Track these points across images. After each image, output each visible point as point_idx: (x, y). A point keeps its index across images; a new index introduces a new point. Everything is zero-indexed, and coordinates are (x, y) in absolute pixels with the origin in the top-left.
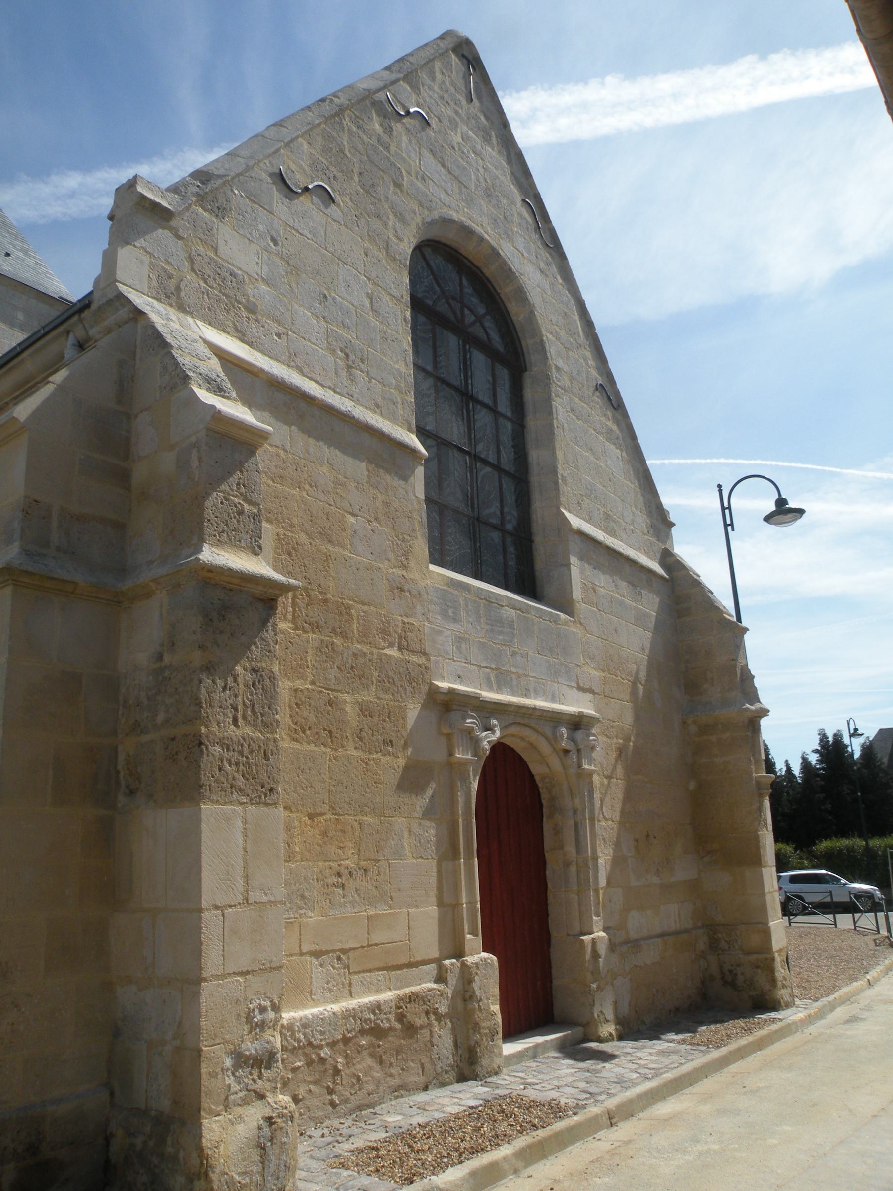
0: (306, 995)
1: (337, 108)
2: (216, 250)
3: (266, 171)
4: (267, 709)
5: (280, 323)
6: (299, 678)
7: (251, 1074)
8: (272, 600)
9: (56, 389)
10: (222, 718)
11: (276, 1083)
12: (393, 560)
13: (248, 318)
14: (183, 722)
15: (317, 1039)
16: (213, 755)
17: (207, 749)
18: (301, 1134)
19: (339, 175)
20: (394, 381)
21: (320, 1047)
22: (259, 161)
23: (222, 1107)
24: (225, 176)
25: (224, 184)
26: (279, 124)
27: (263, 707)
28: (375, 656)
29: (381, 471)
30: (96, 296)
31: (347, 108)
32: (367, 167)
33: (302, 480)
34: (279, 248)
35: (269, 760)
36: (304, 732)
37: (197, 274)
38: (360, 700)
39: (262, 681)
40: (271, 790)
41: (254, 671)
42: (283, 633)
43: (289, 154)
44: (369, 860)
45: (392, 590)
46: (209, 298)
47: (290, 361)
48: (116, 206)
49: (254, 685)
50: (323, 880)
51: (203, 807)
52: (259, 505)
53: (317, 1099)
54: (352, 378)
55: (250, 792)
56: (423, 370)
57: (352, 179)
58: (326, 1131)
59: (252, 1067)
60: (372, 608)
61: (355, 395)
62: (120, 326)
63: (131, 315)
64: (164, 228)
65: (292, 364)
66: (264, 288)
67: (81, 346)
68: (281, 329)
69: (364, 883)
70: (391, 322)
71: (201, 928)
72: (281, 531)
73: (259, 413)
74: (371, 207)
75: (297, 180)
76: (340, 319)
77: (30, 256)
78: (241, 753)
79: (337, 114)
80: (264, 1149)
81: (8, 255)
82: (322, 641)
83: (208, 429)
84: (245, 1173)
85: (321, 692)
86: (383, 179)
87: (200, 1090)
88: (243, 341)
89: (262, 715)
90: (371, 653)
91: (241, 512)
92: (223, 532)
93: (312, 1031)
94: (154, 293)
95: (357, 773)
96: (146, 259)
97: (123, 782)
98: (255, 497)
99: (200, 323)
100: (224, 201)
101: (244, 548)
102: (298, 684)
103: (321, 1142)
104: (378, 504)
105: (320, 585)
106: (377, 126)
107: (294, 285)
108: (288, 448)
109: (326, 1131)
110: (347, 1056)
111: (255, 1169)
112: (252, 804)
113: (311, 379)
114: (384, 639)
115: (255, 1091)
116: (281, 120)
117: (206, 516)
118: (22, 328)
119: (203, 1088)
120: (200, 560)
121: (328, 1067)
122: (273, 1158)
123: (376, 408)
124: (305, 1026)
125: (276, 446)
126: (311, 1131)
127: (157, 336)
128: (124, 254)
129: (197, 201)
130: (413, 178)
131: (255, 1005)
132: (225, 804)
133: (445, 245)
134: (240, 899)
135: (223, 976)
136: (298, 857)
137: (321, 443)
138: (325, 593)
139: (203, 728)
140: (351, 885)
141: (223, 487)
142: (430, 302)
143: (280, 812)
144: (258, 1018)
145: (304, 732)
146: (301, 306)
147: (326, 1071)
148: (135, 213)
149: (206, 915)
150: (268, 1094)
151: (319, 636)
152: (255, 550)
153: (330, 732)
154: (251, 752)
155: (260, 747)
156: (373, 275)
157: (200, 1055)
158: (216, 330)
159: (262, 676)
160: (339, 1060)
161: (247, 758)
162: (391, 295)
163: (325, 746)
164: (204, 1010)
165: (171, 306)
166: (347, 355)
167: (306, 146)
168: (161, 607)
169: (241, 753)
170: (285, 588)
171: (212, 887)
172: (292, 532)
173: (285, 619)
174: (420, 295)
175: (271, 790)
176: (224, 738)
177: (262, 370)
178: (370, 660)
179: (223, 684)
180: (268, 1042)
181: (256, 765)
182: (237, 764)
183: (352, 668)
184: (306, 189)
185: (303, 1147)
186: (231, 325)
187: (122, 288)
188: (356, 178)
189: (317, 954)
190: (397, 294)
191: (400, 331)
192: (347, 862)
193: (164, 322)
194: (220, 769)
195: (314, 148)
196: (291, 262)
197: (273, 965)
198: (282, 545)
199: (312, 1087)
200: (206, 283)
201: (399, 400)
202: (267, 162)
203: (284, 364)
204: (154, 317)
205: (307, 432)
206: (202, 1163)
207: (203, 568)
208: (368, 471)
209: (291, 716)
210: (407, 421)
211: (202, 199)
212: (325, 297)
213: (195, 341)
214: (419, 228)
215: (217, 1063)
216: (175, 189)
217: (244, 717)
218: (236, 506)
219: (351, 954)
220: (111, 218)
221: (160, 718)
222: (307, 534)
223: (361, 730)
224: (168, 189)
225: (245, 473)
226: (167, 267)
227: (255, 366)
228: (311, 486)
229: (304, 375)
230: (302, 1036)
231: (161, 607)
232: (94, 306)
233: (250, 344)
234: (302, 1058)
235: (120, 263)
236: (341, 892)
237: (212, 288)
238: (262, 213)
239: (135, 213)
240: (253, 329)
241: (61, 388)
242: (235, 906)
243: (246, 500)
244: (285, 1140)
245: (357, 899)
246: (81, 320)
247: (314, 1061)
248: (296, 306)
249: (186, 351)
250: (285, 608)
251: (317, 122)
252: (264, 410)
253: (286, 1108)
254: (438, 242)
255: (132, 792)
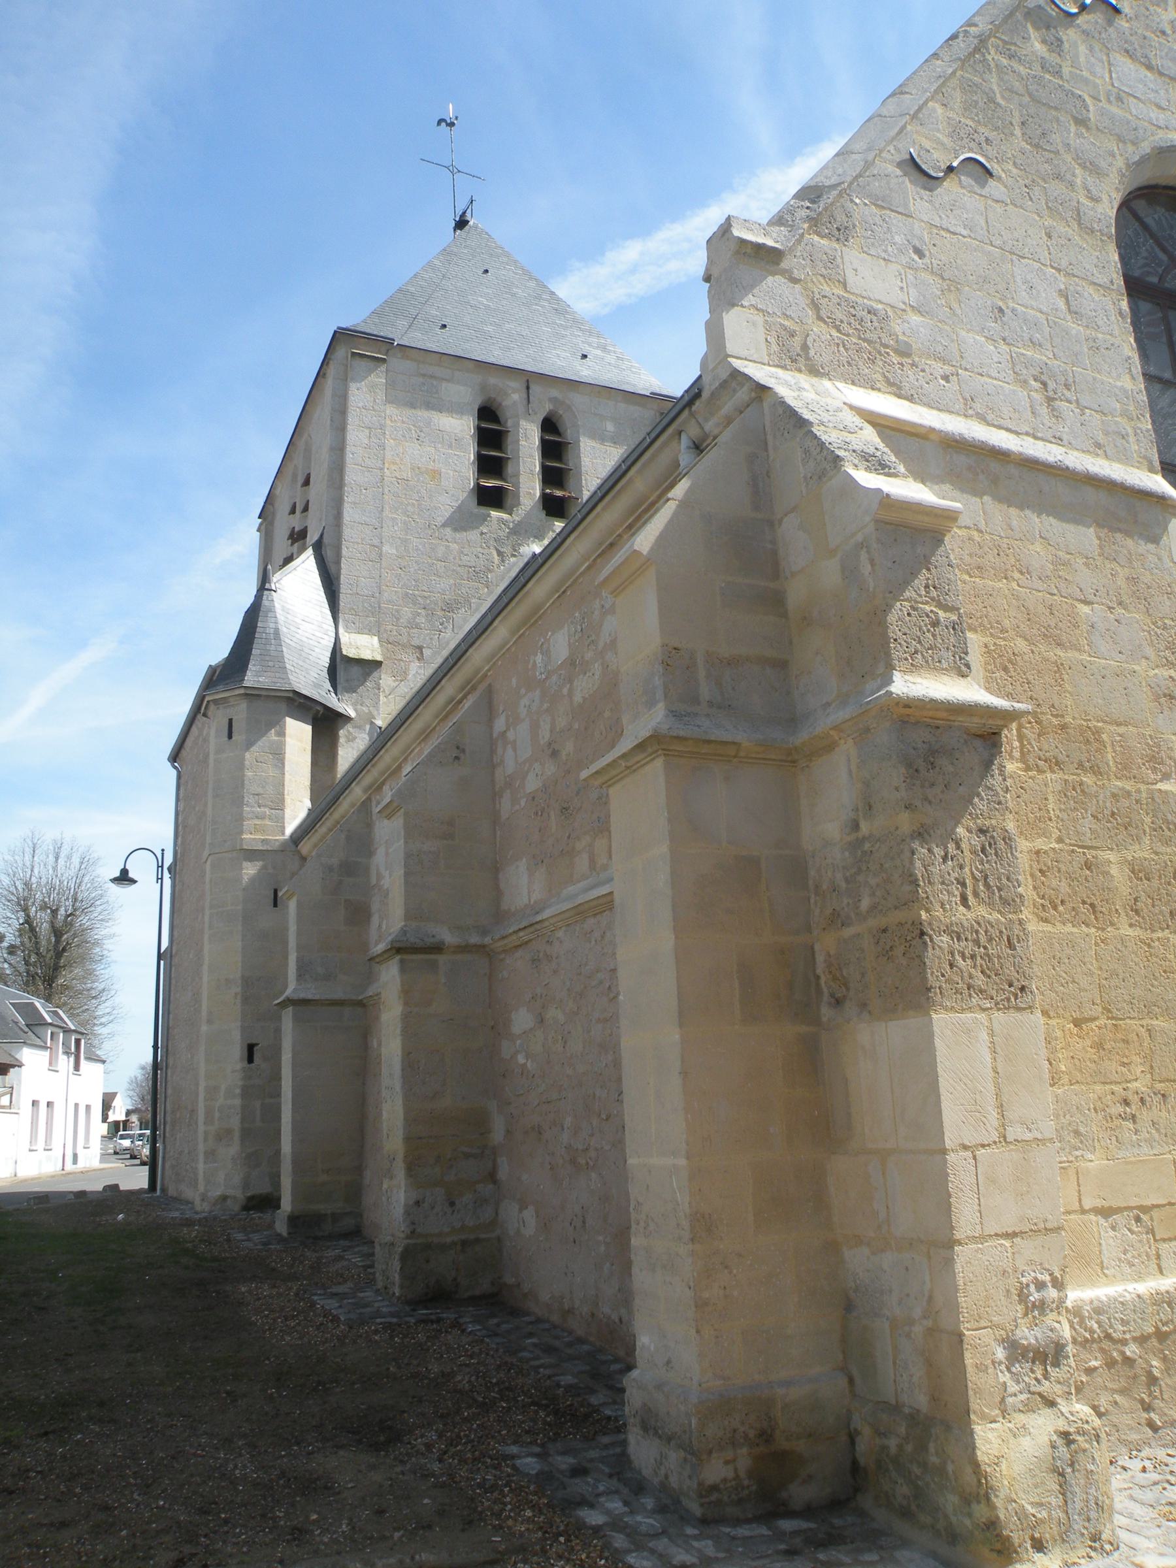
0: (1099, 1270)
1: (976, 41)
2: (845, 285)
3: (891, 162)
4: (1004, 881)
5: (944, 361)
6: (1039, 836)
7: (1033, 1371)
8: (994, 734)
9: (678, 506)
10: (946, 898)
11: (1069, 1386)
12: (1152, 656)
13: (902, 364)
14: (896, 908)
15: (1118, 1331)
16: (940, 947)
17: (932, 940)
18: (1111, 1462)
19: (992, 135)
20: (1118, 405)
21: (1124, 1342)
22: (881, 151)
23: (997, 1412)
24: (840, 184)
25: (840, 195)
26: (899, 92)
27: (999, 879)
28: (1144, 795)
29: (1118, 535)
30: (706, 380)
31: (989, 37)
32: (1032, 111)
33: (1009, 567)
34: (927, 260)
35: (1015, 949)
36: (1055, 908)
37: (825, 322)
38: (1130, 858)
39: (993, 843)
40: (1023, 989)
41: (982, 831)
42: (1011, 777)
43: (919, 128)
44: (1168, 1080)
45: (1157, 699)
46: (846, 350)
47: (968, 407)
48: (711, 261)
49: (983, 850)
50: (1104, 1110)
51: (934, 1016)
52: (958, 609)
53: (1129, 1417)
54: (1056, 415)
55: (994, 993)
56: (1160, 380)
57: (1012, 134)
58: (1147, 1463)
59: (1033, 1362)
60: (1131, 728)
61: (1065, 437)
62: (741, 412)
63: (753, 394)
64: (774, 274)
65: (970, 412)
66: (915, 319)
67: (698, 448)
68: (948, 369)
69: (1164, 1114)
70: (1100, 323)
71: (948, 1175)
72: (988, 639)
73: (936, 487)
74: (1046, 165)
75: (935, 160)
76: (1026, 336)
77: (609, 352)
78: (977, 942)
79: (977, 50)
80: (1062, 1474)
81: (584, 356)
82: (1066, 781)
83: (877, 521)
84: (1041, 1505)
85: (1073, 851)
86: (1058, 120)
87: (966, 1386)
88: (899, 396)
89: (1000, 889)
90: (1139, 791)
91: (936, 623)
92: (916, 652)
93: (1109, 1319)
94: (776, 359)
95: (1137, 960)
96: (759, 319)
97: (825, 990)
98: (950, 600)
99: (840, 385)
100: (844, 217)
101: (946, 669)
102: (1040, 843)
103: (1141, 1478)
104: (1121, 582)
105: (1053, 706)
106: (1038, 46)
107: (955, 305)
108: (982, 526)
109: (1147, 1463)
110: (1164, 1359)
111: (1053, 1501)
112: (999, 1009)
113: (1000, 427)
114: (1154, 770)
115: (1040, 1394)
116: (900, 86)
117: (892, 635)
118: (615, 441)
119: (970, 1384)
120: (892, 693)
121: (1139, 1371)
122: (1077, 1490)
123: (1098, 448)
124: (1098, 1311)
125: (966, 527)
126: (1124, 1461)
127: (791, 413)
128: (733, 320)
129: (810, 227)
130: (1104, 104)
131: (1030, 1278)
132: (963, 1010)
133: (1166, 187)
134: (995, 1136)
135: (982, 1239)
136: (1066, 1079)
137: (1027, 512)
138: (1062, 716)
139: (923, 913)
140: (1145, 1116)
141: (907, 594)
142: (1155, 280)
143: (1038, 1017)
144: (1035, 1296)
145: (1055, 908)
146: (968, 331)
147: (1135, 1377)
148: (737, 263)
149: (951, 1158)
150: (1059, 1400)
151: (1061, 775)
152: (962, 670)
153: (1092, 905)
154: (990, 940)
155: (1001, 932)
156: (1064, 263)
157: (962, 1341)
158: (861, 390)
159: (992, 837)
160: (1154, 1363)
161: (985, 948)
162: (1095, 284)
163: (1087, 925)
164: (961, 1283)
165: (800, 371)
166: (1044, 384)
167: (940, 110)
168: (849, 760)
169: (977, 942)
170: (1009, 716)
171: (957, 1122)
172: (1004, 639)
173: (1012, 757)
174: (1137, 273)
175: (1023, 989)
176: (952, 925)
177: (932, 430)
178: (1137, 801)
179: (943, 853)
180: (1051, 1330)
181: (999, 957)
182: (973, 957)
183: (1113, 814)
184: (950, 169)
185: (1117, 1481)
186: (881, 378)
187: (737, 364)
188: (1018, 132)
189: (1105, 1212)
190: (1103, 280)
191: (1116, 332)
192: (1135, 1084)
193: (796, 394)
194: (951, 965)
195: (952, 109)
196: (946, 276)
197: (1049, 1225)
198: (994, 658)
199: (1117, 1397)
200: (839, 331)
201: (1130, 431)
202: (891, 148)
203: (959, 414)
204: (782, 391)
205: (1007, 500)
206: (979, 1481)
207: (897, 704)
208: (1099, 538)
209: (1035, 888)
210: (1145, 457)
211: (814, 223)
212: (1001, 310)
213: (839, 410)
214: (1123, 175)
215: (985, 1353)
216: (779, 220)
217: (976, 894)
218: (928, 616)
219: (1155, 1213)
220: (707, 278)
221: (865, 903)
222: (1026, 640)
223: (1136, 900)
224: (771, 223)
225: (933, 571)
226: (786, 323)
227: (921, 425)
228: (1021, 573)
229: (989, 424)
230: (1096, 1326)
231: (849, 760)
232: (706, 394)
233: (910, 399)
234: (1098, 1355)
235: (728, 333)
236: (1131, 1126)
237: (848, 335)
238: (895, 219)
239: (737, 263)
240: (910, 378)
241: (684, 504)
242: (989, 1145)
243: (940, 605)
244: (1091, 1467)
245: (1156, 1136)
246: (692, 415)
247: (1116, 1362)
248: (963, 333)
249: (831, 425)
250: (1009, 743)
251: (950, 71)
252: (943, 482)
253: (1087, 1422)
254: (1155, 187)
255: (838, 1002)
